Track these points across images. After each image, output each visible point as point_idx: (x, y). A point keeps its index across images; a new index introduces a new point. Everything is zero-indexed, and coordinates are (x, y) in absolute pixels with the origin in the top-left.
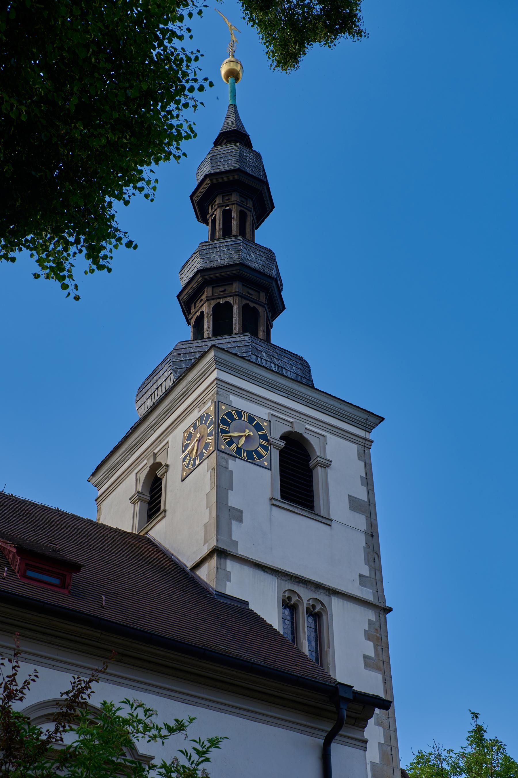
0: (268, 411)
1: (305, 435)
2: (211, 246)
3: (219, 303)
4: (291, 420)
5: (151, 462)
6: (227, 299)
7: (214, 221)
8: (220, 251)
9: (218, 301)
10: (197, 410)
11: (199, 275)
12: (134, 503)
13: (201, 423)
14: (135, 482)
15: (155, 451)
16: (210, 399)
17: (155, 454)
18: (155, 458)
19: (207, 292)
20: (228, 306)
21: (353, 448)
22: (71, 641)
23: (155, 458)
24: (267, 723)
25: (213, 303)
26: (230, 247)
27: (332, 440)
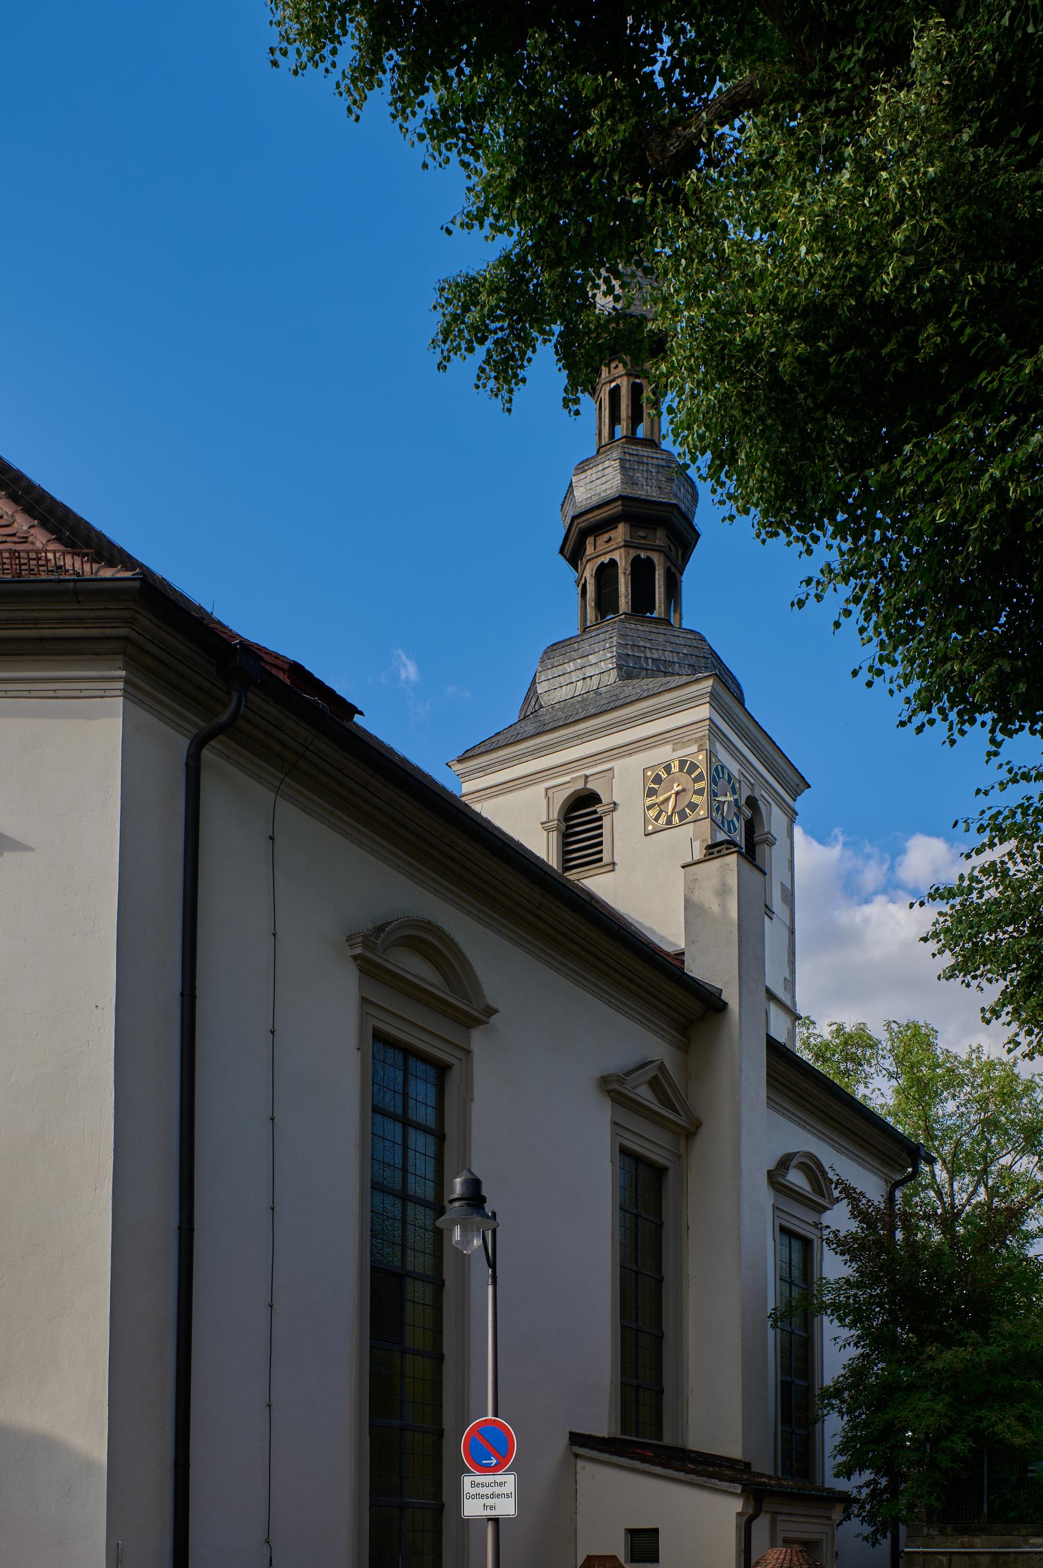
0: (739, 767)
1: (760, 802)
2: (636, 458)
3: (639, 556)
4: (752, 781)
5: (580, 785)
6: (650, 554)
7: (615, 393)
8: (647, 471)
9: (638, 552)
10: (669, 747)
11: (620, 503)
12: (548, 830)
13: (681, 770)
14: (545, 801)
15: (588, 772)
16: (696, 742)
17: (587, 777)
18: (586, 782)
19: (620, 533)
20: (649, 563)
21: (785, 818)
22: (797, 1094)
23: (586, 782)
24: (868, 1169)
25: (633, 553)
26: (661, 470)
27: (775, 808)
